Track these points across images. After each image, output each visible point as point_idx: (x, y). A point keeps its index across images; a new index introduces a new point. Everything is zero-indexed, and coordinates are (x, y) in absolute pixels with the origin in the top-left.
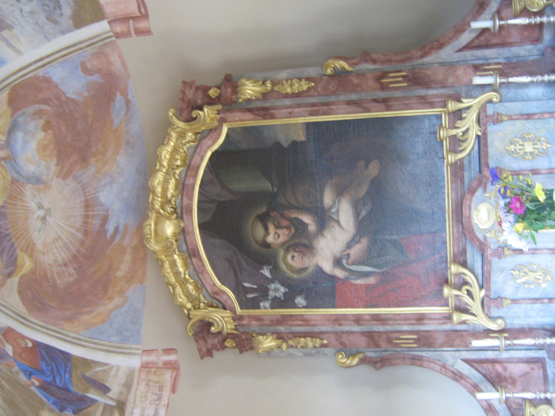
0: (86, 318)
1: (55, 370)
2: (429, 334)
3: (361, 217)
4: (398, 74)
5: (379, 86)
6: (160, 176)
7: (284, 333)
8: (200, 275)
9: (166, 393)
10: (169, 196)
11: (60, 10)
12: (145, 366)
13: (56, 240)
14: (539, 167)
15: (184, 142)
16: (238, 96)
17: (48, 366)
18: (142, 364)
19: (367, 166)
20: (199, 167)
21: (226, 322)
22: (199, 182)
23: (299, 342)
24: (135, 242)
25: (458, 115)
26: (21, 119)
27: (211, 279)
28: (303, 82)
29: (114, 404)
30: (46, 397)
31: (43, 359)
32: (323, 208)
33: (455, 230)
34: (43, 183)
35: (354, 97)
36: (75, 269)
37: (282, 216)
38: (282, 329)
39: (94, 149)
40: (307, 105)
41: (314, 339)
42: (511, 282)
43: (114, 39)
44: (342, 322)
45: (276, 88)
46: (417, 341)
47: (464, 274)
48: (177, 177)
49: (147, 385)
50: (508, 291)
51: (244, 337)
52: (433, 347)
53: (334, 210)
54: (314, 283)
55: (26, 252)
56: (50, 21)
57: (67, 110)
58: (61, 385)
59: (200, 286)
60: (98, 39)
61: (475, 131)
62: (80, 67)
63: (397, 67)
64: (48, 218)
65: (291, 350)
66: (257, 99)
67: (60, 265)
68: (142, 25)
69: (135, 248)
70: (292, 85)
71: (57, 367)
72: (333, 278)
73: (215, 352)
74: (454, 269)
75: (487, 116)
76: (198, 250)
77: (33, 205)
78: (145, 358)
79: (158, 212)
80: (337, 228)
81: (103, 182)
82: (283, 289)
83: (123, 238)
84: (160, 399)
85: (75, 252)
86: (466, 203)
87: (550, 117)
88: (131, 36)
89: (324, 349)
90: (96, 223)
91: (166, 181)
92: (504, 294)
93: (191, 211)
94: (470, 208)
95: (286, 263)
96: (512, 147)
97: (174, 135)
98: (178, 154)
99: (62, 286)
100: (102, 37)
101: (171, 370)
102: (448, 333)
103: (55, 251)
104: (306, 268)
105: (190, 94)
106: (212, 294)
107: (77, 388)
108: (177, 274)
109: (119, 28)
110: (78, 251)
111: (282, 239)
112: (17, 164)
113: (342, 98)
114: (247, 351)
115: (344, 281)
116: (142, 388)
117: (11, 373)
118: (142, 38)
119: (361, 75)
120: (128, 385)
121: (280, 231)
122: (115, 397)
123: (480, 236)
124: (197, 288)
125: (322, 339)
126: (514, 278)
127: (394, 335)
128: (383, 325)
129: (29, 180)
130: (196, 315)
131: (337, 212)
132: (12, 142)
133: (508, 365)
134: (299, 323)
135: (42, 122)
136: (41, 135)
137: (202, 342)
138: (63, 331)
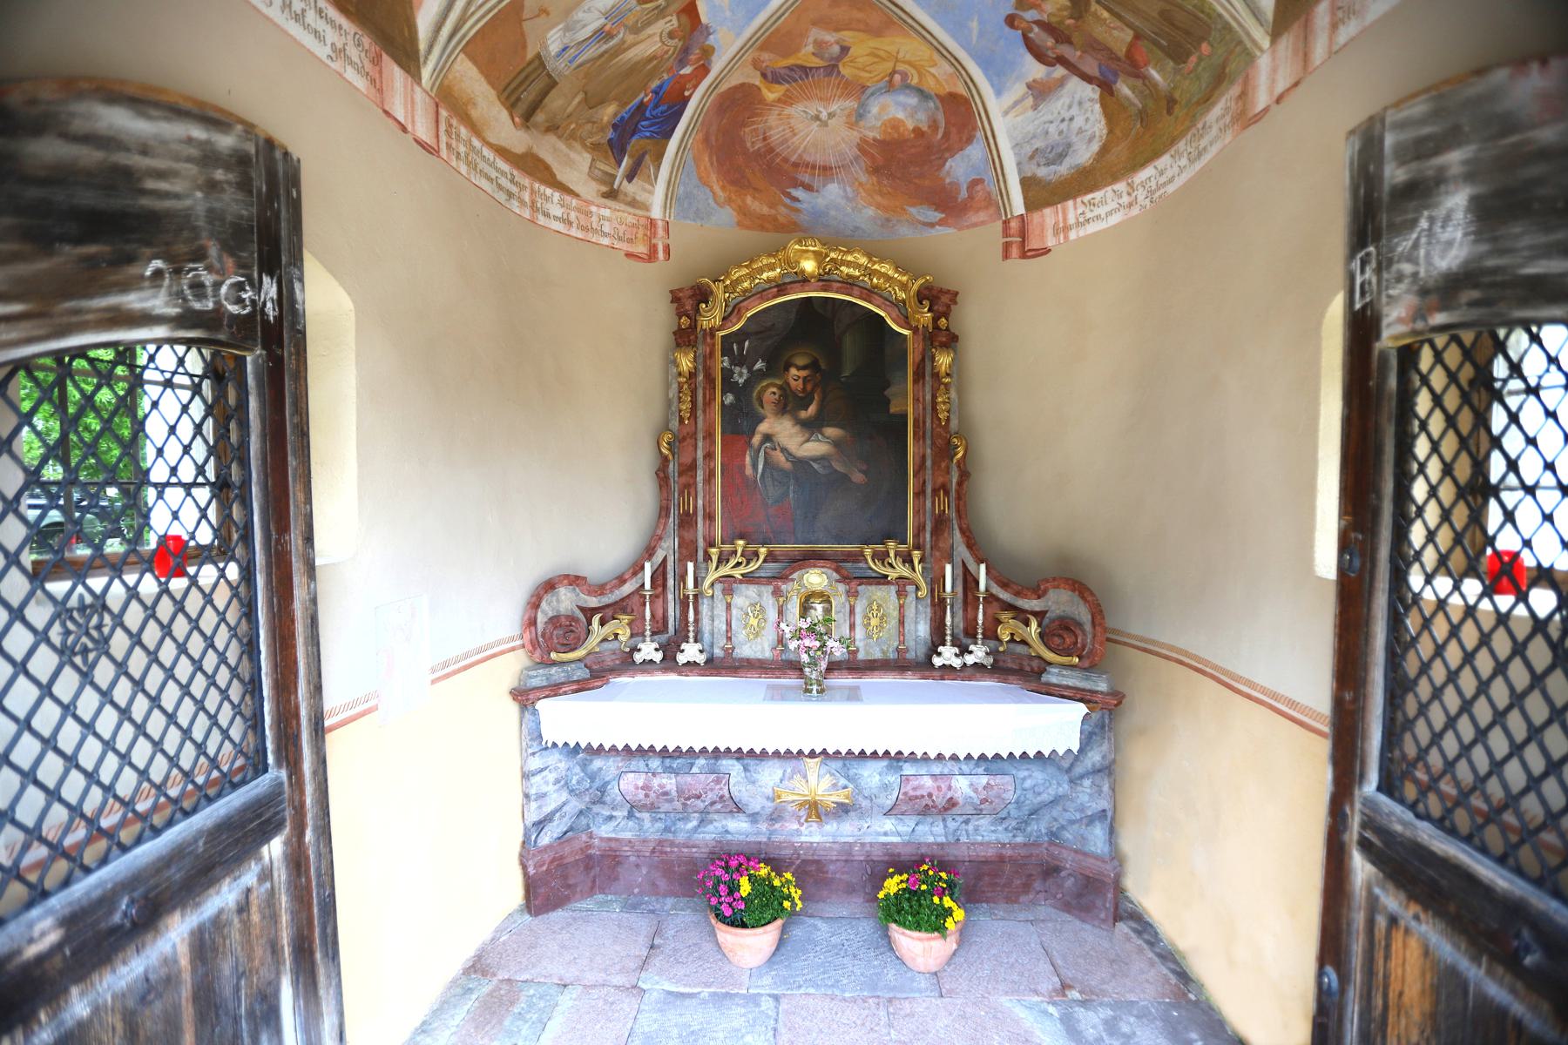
6: (863, 260)
9: (625, 247)
10: (843, 268)
12: (652, 223)
15: (897, 288)
17: (662, 113)
19: (860, 471)
20: (870, 302)
24: (781, 219)
25: (908, 560)
26: (931, 104)
29: (615, 187)
31: (669, 108)
32: (823, 426)
34: (857, 122)
35: (929, 463)
36: (759, 149)
37: (816, 386)
38: (701, 377)
40: (924, 417)
42: (747, 603)
45: (942, 387)
46: (687, 513)
51: (692, 337)
52: (679, 527)
53: (820, 437)
54: (748, 413)
55: (783, 95)
57: (933, 157)
59: (748, 295)
60: (1006, 201)
63: (953, 505)
66: (933, 368)
68: (1015, 251)
69: (775, 219)
70: (944, 403)
71: (658, 123)
72: (752, 433)
74: (763, 551)
77: (834, 107)
79: (827, 256)
81: (848, 189)
82: (741, 381)
83: (786, 206)
84: (620, 239)
91: (857, 266)
93: (825, 291)
95: (768, 386)
96: (875, 607)
97: (905, 279)
100: (1007, 206)
105: (945, 299)
107: (635, 143)
108: (761, 270)
109: (1014, 225)
110: (778, 155)
111: (793, 383)
115: (749, 445)
116: (630, 219)
120: (633, 203)
121: (801, 381)
123: (795, 576)
124: (745, 291)
125: (689, 419)
129: (862, 105)
130: (718, 288)
131: (819, 441)
132: (908, 91)
133: (661, 600)
135: (925, 129)
136: (910, 125)
137: (690, 293)
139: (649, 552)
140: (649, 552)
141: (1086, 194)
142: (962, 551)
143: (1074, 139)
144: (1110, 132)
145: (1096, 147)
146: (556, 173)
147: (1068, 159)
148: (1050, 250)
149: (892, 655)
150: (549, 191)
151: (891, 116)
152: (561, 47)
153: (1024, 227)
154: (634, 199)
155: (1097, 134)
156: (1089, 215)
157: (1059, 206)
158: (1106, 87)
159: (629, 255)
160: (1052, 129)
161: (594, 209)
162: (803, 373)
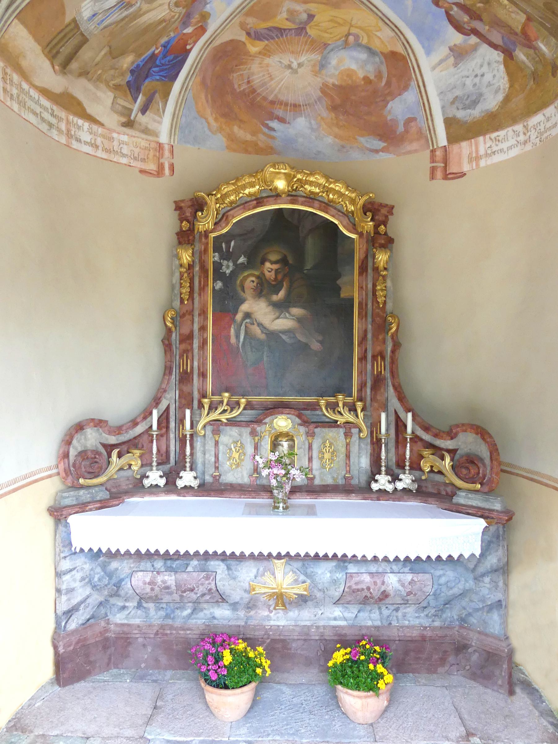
0: (203, 96)
1: (165, 67)
2: (191, 381)
3: (281, 335)
4: (383, 368)
5: (376, 354)
7: (193, 270)
8: (242, 207)
10: (306, 186)
11: (462, 109)
12: (160, 146)
13: (271, 76)
14: (313, 462)
15: (347, 203)
16: (378, 248)
17: (169, 61)
18: (162, 144)
20: (327, 213)
21: (205, 224)
22: (315, 212)
23: (185, 281)
25: (352, 409)
26: (377, 59)
27: (238, 215)
28: (383, 299)
29: (132, 118)
30: (144, 60)
32: (289, 307)
33: (269, 403)
35: (369, 336)
36: (244, 90)
37: (285, 276)
38: (197, 268)
39: (341, 117)
41: (188, 293)
42: (231, 441)
43: (431, 148)
44: (202, 317)
45: (381, 278)
46: (185, 372)
47: (239, 408)
48: (320, 194)
49: (146, 148)
50: (224, 439)
51: (191, 238)
52: (180, 382)
53: (287, 315)
56: (454, 99)
57: (378, 100)
58: (151, 71)
59: (234, 206)
61: (341, 420)
62: (413, 116)
64: (290, 70)
65: (177, 275)
66: (374, 263)
67: (248, 78)
68: (439, 174)
69: (256, 145)
70: (382, 290)
71: (166, 69)
72: (236, 312)
73: (178, 212)
75: (350, 428)
76: (262, 206)
77: (303, 59)
78: (166, 147)
80: (274, 317)
82: (228, 272)
83: (264, 134)
84: (135, 159)
85: (258, 91)
86: (293, 411)
87: (346, 471)
88: (431, 163)
89: (179, 300)
90: (280, 112)
91: (318, 185)
92: (222, 436)
94: (288, 414)
95: (248, 276)
96: (328, 444)
97: (353, 195)
98: (338, 197)
99: (231, 78)
101: (157, 170)
102: (191, 394)
103: (261, 75)
104: (244, 292)
105: (384, 211)
106: (227, 214)
107: (147, 85)
108: (244, 187)
109: (439, 153)
110: (259, 94)
111: (267, 274)
112: (340, 50)
113: (370, 327)
114: (178, 238)
115: (233, 320)
116: (144, 144)
117: (171, 31)
118: (428, 172)
119: (384, 342)
120: (146, 131)
121: (273, 272)
122: (137, 119)
123: (267, 420)
124: (232, 203)
126: (235, 442)
127: (190, 355)
128: (199, 347)
129: (325, 58)
130: (211, 201)
131: (286, 318)
134: (202, 283)
135: (372, 77)
136: (361, 74)
138: (194, 76)
139: (156, 401)
140: (156, 401)
141: (492, 132)
142: (394, 403)
143: (484, 90)
144: (511, 86)
145: (500, 97)
146: (86, 107)
147: (480, 105)
148: (465, 174)
149: (341, 482)
150: (80, 122)
151: (346, 67)
152: (92, 13)
153: (446, 155)
154: (147, 128)
155: (502, 88)
156: (495, 148)
157: (473, 140)
158: (508, 54)
159: (142, 171)
160: (468, 82)
161: (115, 135)
162: (275, 267)
